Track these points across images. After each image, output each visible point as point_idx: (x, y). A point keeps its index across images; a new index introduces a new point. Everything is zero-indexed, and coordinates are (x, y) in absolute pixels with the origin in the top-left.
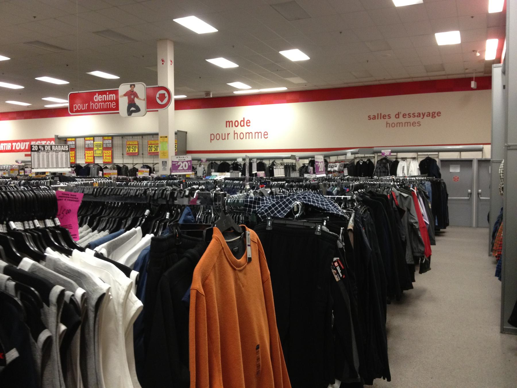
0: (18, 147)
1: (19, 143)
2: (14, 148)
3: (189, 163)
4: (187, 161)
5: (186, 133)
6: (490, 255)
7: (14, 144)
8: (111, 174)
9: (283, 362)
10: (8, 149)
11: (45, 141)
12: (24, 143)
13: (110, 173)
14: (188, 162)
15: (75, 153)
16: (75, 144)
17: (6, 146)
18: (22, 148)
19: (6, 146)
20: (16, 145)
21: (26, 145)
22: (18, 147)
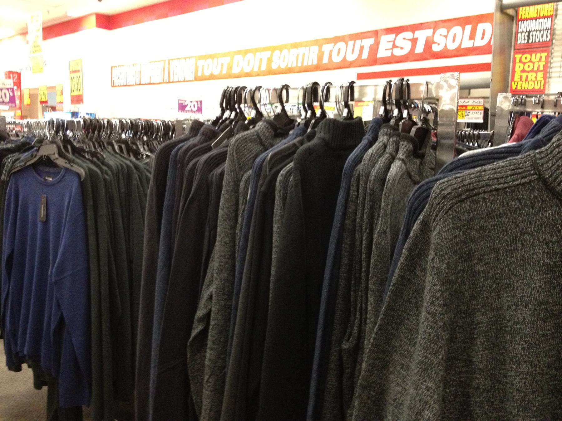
0: (338, 54)
1: (341, 45)
2: (325, 61)
3: (10, 91)
4: (8, 89)
5: (19, 75)
6: (163, 122)
7: (327, 48)
8: (468, 108)
9: (53, 260)
10: (310, 64)
11: (429, 28)
12: (358, 42)
13: (466, 106)
14: (8, 91)
15: (547, 58)
16: (552, 30)
17: (304, 54)
18: (351, 57)
19: (304, 54)
20: (331, 51)
21: (362, 48)
22: (338, 54)
